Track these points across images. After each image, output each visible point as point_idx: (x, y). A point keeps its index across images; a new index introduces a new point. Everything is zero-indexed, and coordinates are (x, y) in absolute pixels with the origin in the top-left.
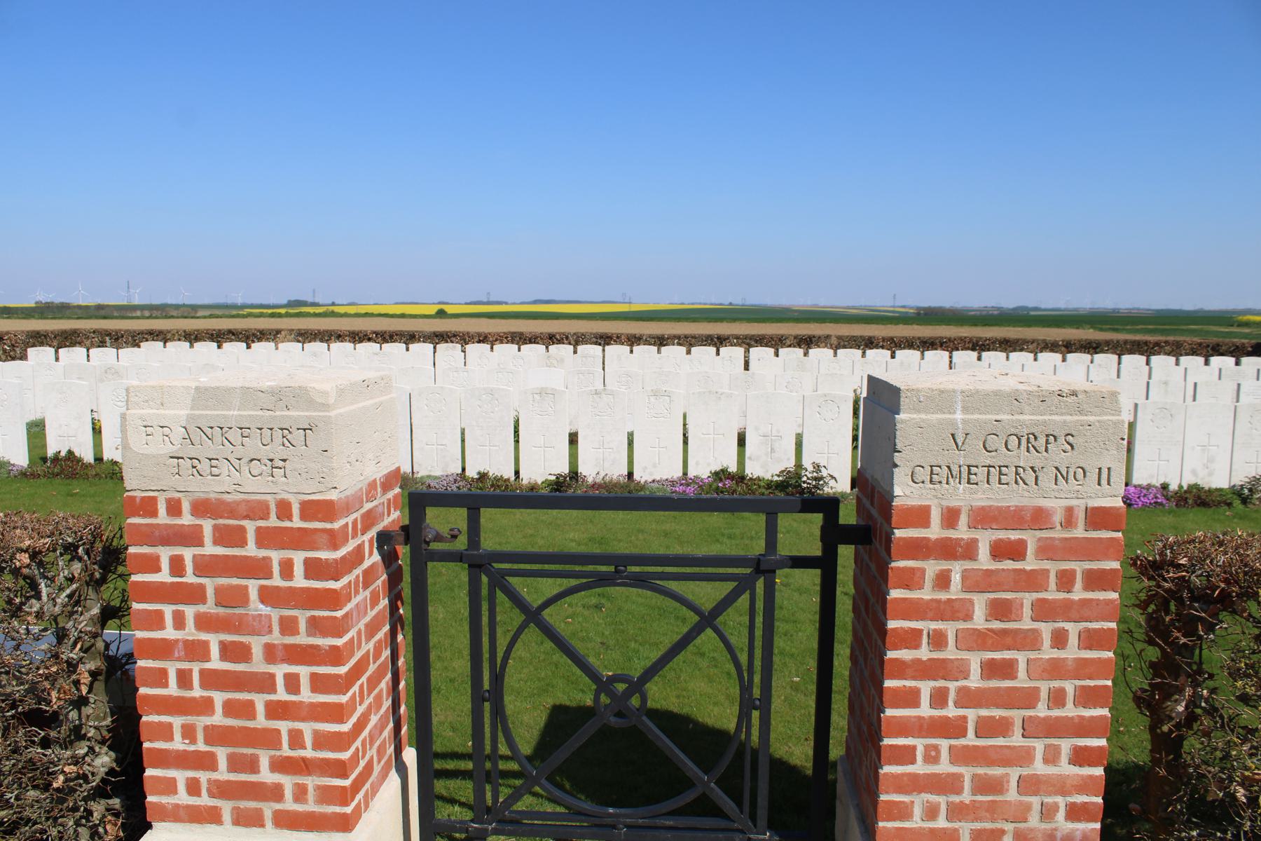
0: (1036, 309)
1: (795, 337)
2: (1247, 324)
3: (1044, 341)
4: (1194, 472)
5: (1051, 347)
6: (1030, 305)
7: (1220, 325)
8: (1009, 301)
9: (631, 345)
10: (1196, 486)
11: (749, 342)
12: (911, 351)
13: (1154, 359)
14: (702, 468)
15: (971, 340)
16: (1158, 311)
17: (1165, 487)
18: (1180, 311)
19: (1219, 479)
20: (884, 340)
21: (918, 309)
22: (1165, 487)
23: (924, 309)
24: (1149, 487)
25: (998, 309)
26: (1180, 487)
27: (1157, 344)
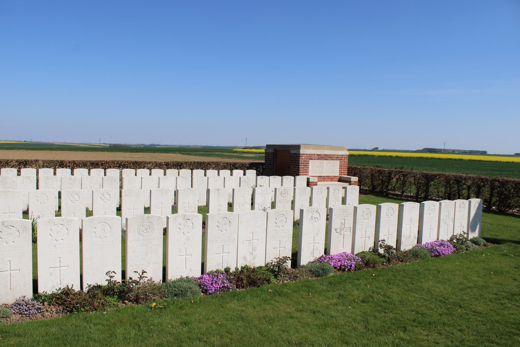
0: (158, 145)
1: (17, 161)
2: (236, 152)
3: (155, 162)
4: (245, 258)
5: (159, 165)
6: (156, 144)
7: (227, 152)
8: (147, 141)
9: (150, 169)
10: (245, 269)
11: (121, 165)
12: (65, 169)
13: (208, 171)
14: (96, 277)
15: (118, 162)
16: (204, 146)
17: (227, 270)
18: (212, 147)
19: (258, 261)
20: (70, 162)
21: (110, 144)
22: (227, 270)
23: (113, 145)
24: (217, 271)
25: (143, 145)
26: (237, 269)
27: (209, 163)
